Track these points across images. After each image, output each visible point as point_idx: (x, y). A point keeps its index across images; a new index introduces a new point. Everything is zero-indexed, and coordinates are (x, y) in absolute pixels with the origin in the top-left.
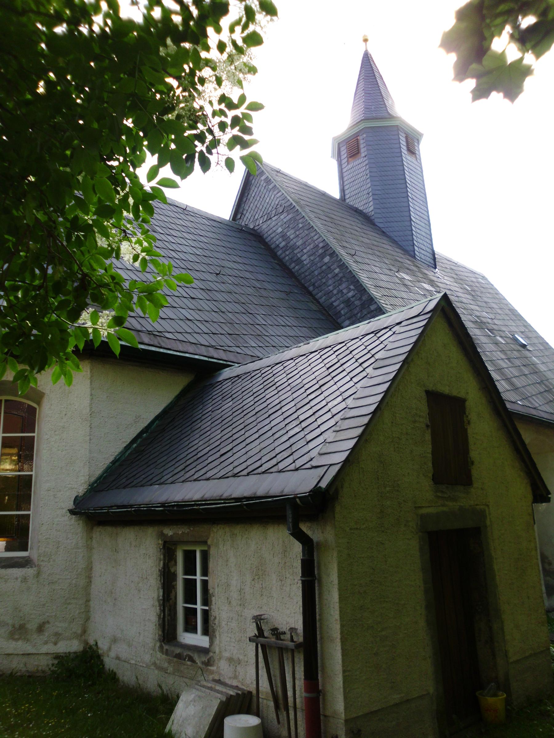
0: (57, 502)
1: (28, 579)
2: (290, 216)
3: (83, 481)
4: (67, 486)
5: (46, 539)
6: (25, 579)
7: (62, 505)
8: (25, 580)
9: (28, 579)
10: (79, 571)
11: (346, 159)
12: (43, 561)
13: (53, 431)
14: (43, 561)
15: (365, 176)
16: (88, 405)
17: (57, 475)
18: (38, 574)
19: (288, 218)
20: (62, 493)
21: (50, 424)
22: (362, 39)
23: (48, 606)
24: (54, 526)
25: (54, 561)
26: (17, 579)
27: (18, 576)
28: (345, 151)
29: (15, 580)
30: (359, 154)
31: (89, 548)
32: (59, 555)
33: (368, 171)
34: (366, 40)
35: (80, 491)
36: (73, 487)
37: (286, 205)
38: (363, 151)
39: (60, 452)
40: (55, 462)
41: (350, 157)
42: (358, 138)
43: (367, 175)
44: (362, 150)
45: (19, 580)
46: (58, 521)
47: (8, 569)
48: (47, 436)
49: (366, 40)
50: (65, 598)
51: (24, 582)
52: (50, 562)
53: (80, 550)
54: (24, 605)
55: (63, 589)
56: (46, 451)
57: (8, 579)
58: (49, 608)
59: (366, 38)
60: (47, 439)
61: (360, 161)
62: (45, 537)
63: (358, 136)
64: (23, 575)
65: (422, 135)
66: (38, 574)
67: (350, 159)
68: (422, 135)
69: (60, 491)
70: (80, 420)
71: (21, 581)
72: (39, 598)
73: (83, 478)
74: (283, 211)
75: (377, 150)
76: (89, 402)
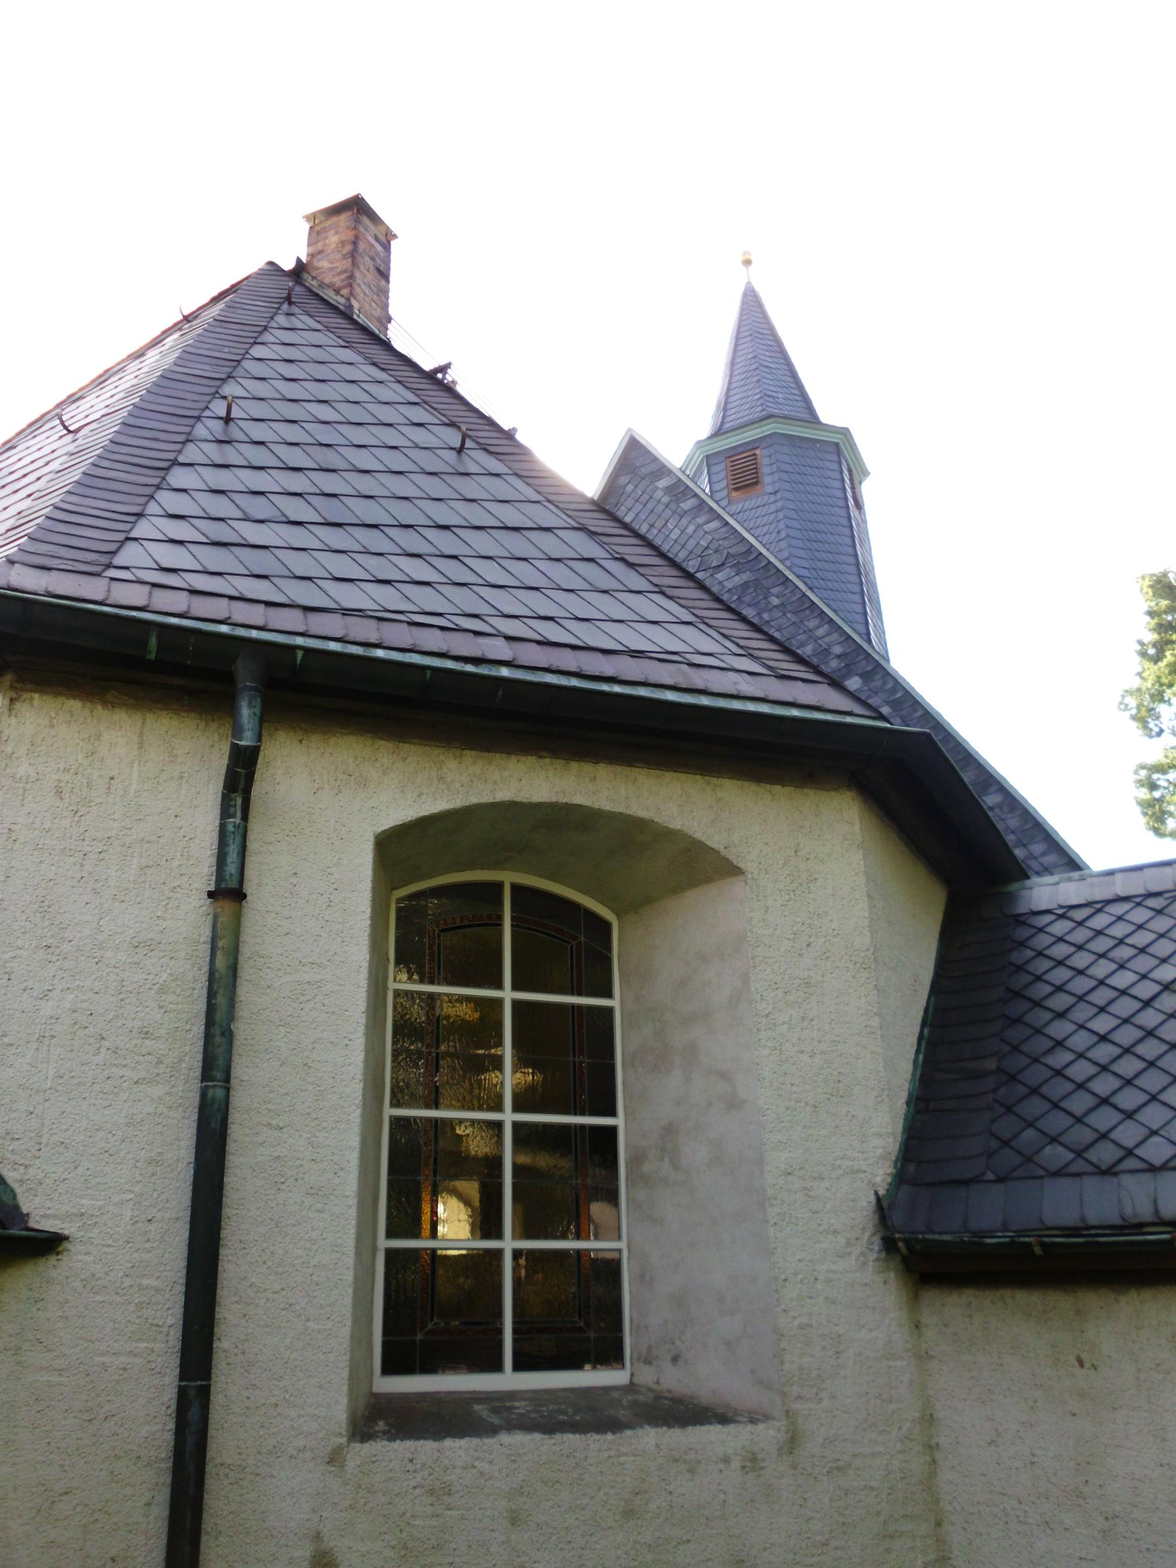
0: (816, 1212)
1: (763, 1460)
2: (745, 577)
3: (880, 1151)
4: (838, 1163)
5: (801, 1327)
6: (754, 1459)
7: (833, 1221)
8: (752, 1463)
9: (763, 1460)
10: (905, 1428)
11: (725, 493)
12: (799, 1397)
13: (780, 992)
14: (799, 1397)
15: (774, 535)
16: (866, 922)
17: (804, 1127)
18: (792, 1443)
19: (737, 580)
20: (826, 1184)
21: (769, 970)
22: (741, 259)
23: (837, 1548)
24: (819, 1286)
25: (833, 1397)
26: (726, 1460)
27: (730, 1451)
28: (723, 474)
29: (722, 1466)
30: (758, 487)
31: (923, 1357)
32: (845, 1377)
33: (782, 525)
34: (747, 263)
35: (878, 1179)
36: (856, 1167)
37: (732, 551)
38: (768, 480)
39: (805, 1057)
40: (794, 1088)
41: (736, 489)
42: (757, 452)
43: (778, 532)
44: (767, 479)
45: (736, 1464)
46: (827, 1271)
47: (690, 1428)
48: (764, 1005)
49: (747, 263)
50: (882, 1518)
51: (754, 1469)
52: (820, 1401)
53: (899, 1364)
54: (765, 1549)
55: (872, 1488)
56: (766, 1052)
57: (699, 1462)
58: (839, 1553)
59: (748, 257)
60: (767, 1016)
61: (759, 501)
62: (796, 1323)
63: (757, 448)
64: (743, 1447)
65: (869, 473)
66: (792, 1443)
67: (735, 494)
68: (869, 473)
69: (821, 1178)
70: (851, 965)
71: (744, 1467)
72: (807, 1521)
73: (878, 1142)
74: (723, 564)
75: (800, 486)
76: (867, 915)
